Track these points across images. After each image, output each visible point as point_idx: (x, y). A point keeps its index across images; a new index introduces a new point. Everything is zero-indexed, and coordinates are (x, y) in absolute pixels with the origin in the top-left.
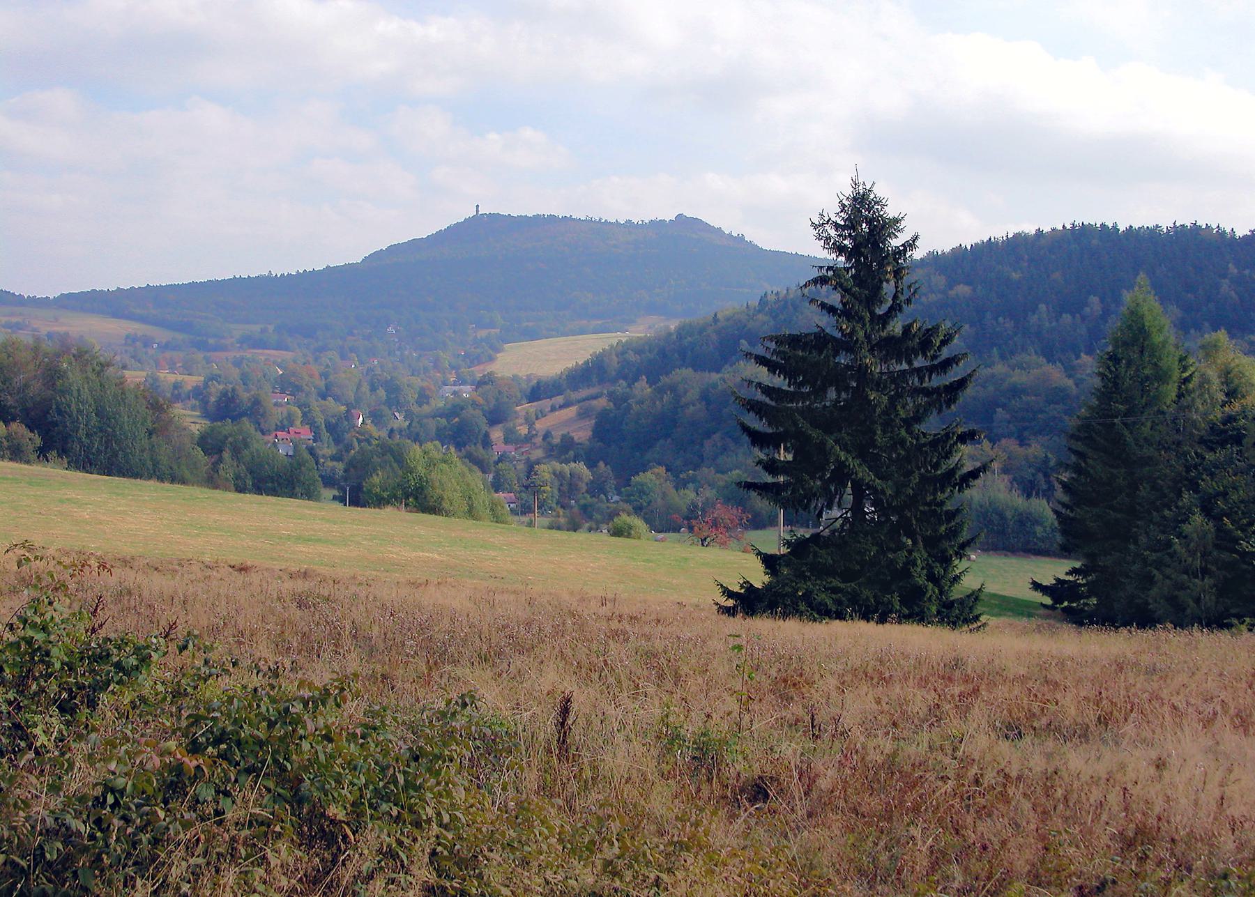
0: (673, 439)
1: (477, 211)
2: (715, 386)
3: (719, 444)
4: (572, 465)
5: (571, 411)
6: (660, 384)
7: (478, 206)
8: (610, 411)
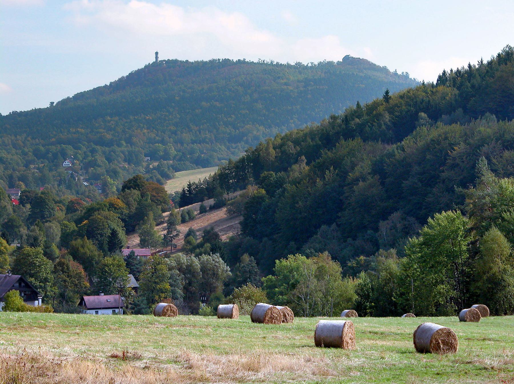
0: (338, 226)
1: (157, 58)
2: (391, 155)
3: (398, 225)
4: (205, 257)
5: (221, 214)
6: (320, 160)
7: (157, 53)
8: (262, 198)
